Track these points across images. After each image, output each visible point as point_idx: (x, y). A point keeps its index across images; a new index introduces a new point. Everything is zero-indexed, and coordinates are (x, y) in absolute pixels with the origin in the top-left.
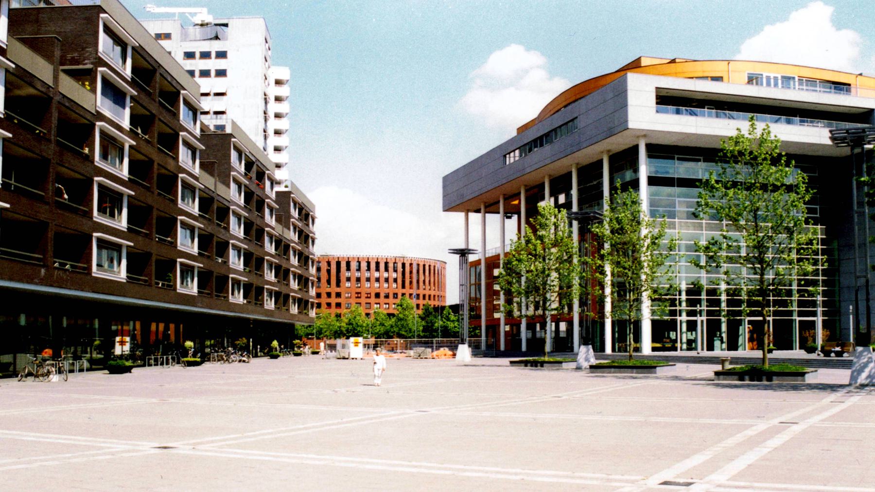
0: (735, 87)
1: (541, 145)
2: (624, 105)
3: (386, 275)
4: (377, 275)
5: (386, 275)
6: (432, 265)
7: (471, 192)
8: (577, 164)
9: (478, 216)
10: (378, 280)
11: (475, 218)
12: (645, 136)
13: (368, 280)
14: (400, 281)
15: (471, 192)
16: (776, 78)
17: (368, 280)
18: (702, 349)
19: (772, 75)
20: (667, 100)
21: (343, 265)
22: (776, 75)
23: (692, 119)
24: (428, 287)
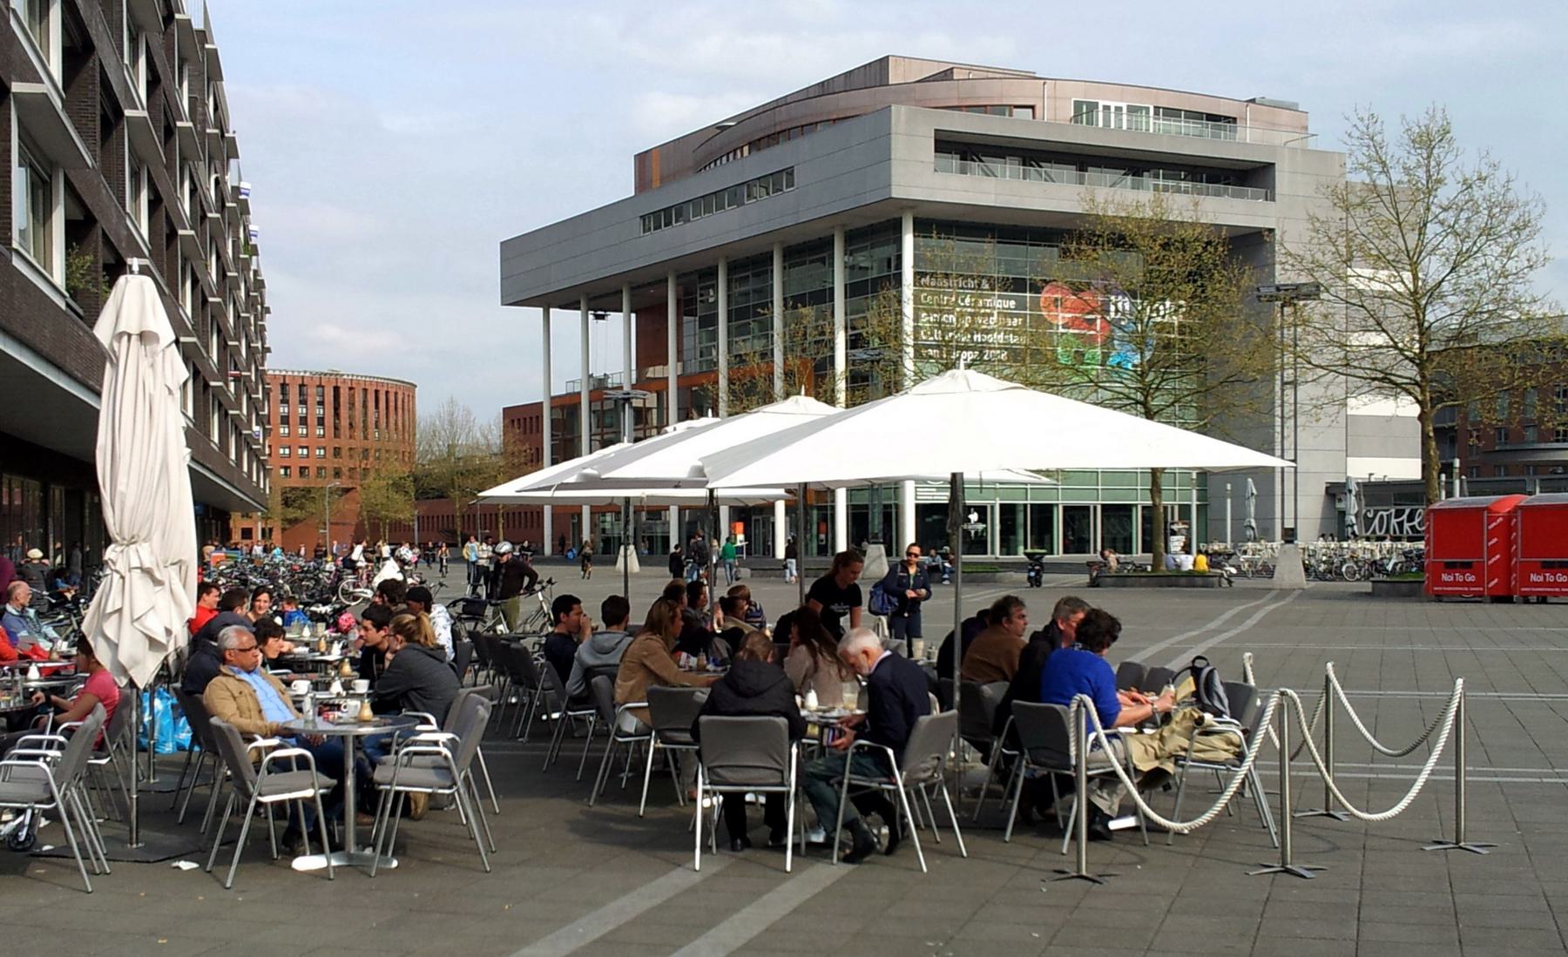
0: (1053, 121)
1: (720, 207)
2: (885, 158)
3: (302, 411)
4: (283, 410)
5: (302, 411)
6: (392, 391)
7: (548, 273)
8: (782, 242)
9: (575, 316)
10: (304, 421)
11: (566, 321)
12: (912, 208)
13: (285, 420)
14: (329, 420)
15: (548, 273)
16: (1118, 109)
17: (285, 420)
18: (992, 507)
19: (1113, 105)
20: (946, 144)
21: (344, 393)
22: (1119, 104)
23: (989, 183)
24: (359, 434)
